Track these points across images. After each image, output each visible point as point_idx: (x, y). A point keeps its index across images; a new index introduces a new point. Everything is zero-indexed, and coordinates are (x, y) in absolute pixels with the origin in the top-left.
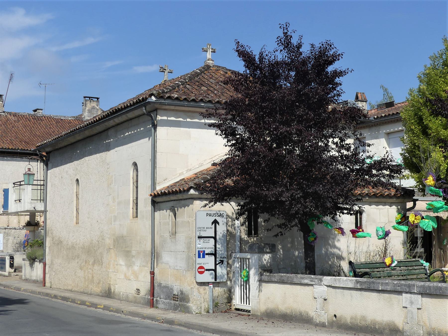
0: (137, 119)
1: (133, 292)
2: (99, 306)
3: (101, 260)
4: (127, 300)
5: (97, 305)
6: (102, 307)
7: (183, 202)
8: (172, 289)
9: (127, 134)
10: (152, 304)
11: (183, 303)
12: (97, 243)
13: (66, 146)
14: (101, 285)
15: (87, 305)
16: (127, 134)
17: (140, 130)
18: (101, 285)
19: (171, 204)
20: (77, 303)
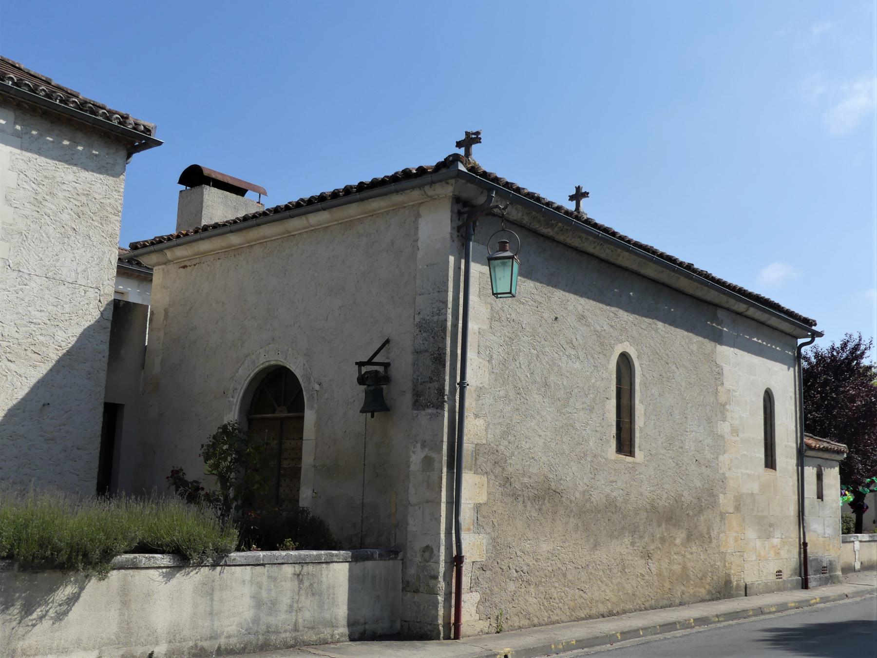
0: (790, 337)
1: (773, 577)
2: (812, 602)
3: (708, 533)
4: (769, 590)
5: (808, 601)
6: (818, 600)
7: (829, 462)
8: (821, 561)
9: (755, 339)
10: (805, 585)
11: (441, 628)
12: (695, 501)
13: (592, 256)
14: (709, 580)
15: (792, 608)
16: (755, 339)
17: (775, 349)
18: (709, 580)
19: (820, 461)
20: (770, 613)
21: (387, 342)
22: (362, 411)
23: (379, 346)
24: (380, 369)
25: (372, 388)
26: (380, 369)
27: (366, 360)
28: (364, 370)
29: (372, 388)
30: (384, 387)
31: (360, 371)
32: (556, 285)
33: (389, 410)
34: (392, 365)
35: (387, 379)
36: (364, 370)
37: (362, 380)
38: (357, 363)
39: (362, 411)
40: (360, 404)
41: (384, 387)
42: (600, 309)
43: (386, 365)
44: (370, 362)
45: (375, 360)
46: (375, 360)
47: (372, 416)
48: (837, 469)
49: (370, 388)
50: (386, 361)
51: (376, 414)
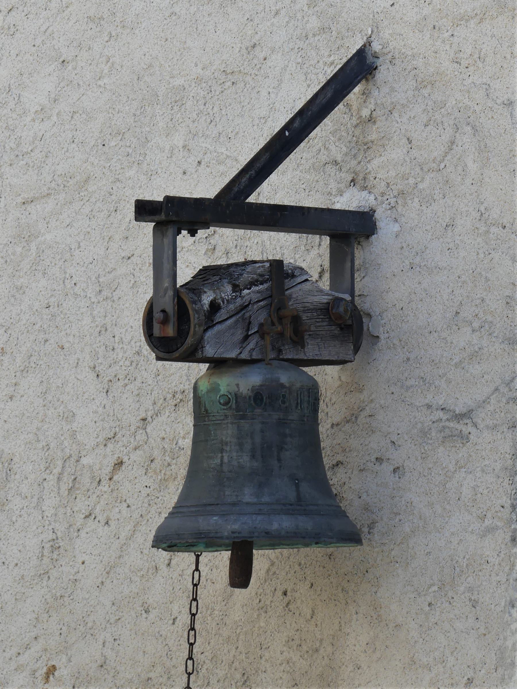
21: (359, 69)
22: (167, 540)
23: (298, 94)
24: (307, 254)
25: (249, 381)
26: (307, 254)
27: (207, 187)
28: (194, 253)
29: (249, 381)
30: (327, 377)
31: (164, 261)
32: (261, 204)
33: (353, 537)
34: (386, 227)
35: (348, 326)
36: (194, 253)
37: (174, 327)
38: (144, 210)
39: (167, 540)
40: (156, 493)
41: (327, 377)
42: (139, 319)
43: (348, 231)
44: (234, 206)
45: (272, 191)
46: (272, 191)
47: (241, 574)
48: (226, 555)
49: (226, 383)
50: (349, 201)
51: (261, 559)
